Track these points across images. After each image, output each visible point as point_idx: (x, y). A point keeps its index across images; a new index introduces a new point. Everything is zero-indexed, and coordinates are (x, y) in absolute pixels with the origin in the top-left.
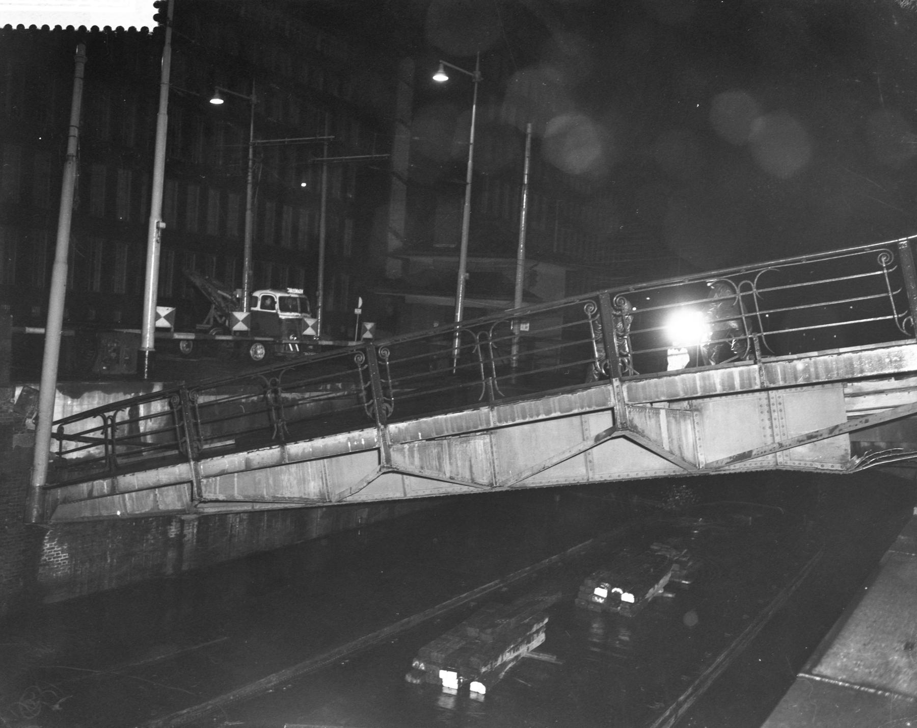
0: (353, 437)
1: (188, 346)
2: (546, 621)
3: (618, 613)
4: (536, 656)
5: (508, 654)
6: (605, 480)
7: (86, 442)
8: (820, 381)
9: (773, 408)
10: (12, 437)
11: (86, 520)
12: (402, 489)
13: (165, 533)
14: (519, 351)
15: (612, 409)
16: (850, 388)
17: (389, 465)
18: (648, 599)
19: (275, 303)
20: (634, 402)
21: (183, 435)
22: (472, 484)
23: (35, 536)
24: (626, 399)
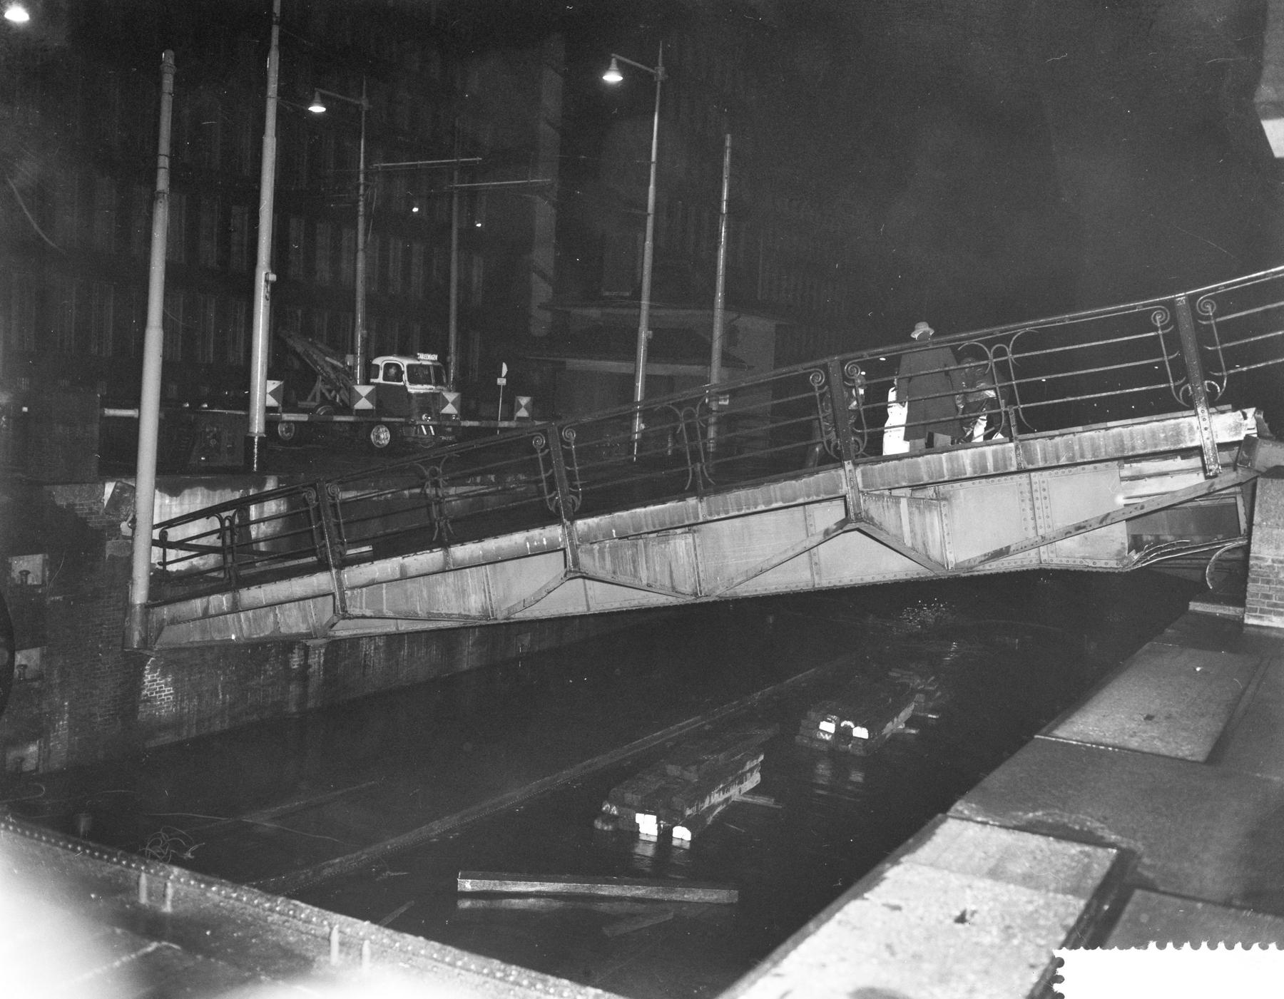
0: (532, 537)
1: (288, 430)
2: (762, 758)
3: (847, 752)
4: (750, 800)
5: (716, 795)
6: (835, 586)
7: (190, 550)
8: (1085, 460)
9: (1036, 495)
10: (105, 544)
11: (196, 645)
12: (585, 603)
13: (286, 663)
14: (718, 433)
15: (844, 497)
16: (1128, 470)
17: (577, 569)
18: (886, 735)
19: (403, 372)
20: (868, 490)
21: (323, 538)
22: (673, 594)
23: (134, 665)
24: (860, 486)
